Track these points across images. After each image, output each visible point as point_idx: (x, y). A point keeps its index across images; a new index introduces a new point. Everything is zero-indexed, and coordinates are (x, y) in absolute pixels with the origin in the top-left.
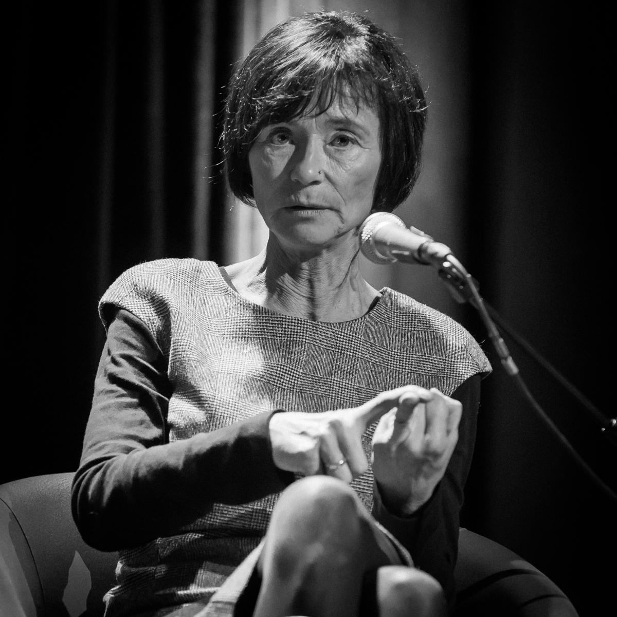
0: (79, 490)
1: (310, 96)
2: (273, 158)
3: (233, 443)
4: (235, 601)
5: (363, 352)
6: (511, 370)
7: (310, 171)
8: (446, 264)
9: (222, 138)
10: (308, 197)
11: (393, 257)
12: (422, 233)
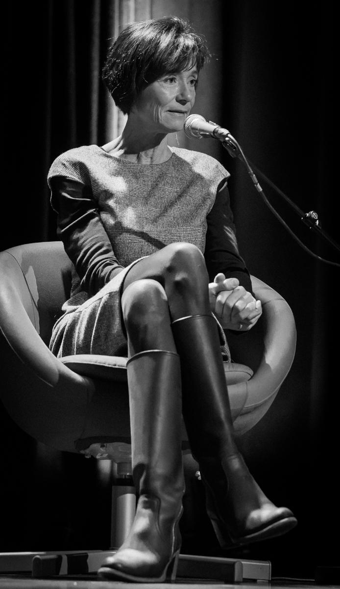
6: (259, 189)
8: (227, 139)
12: (215, 124)
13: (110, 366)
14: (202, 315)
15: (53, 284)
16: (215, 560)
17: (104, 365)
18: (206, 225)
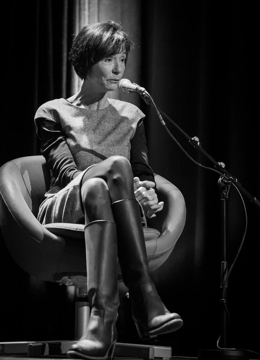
0: (61, 166)
8: (144, 93)
9: (219, 181)
11: (128, 92)
12: (137, 84)
17: (70, 229)
18: (130, 145)
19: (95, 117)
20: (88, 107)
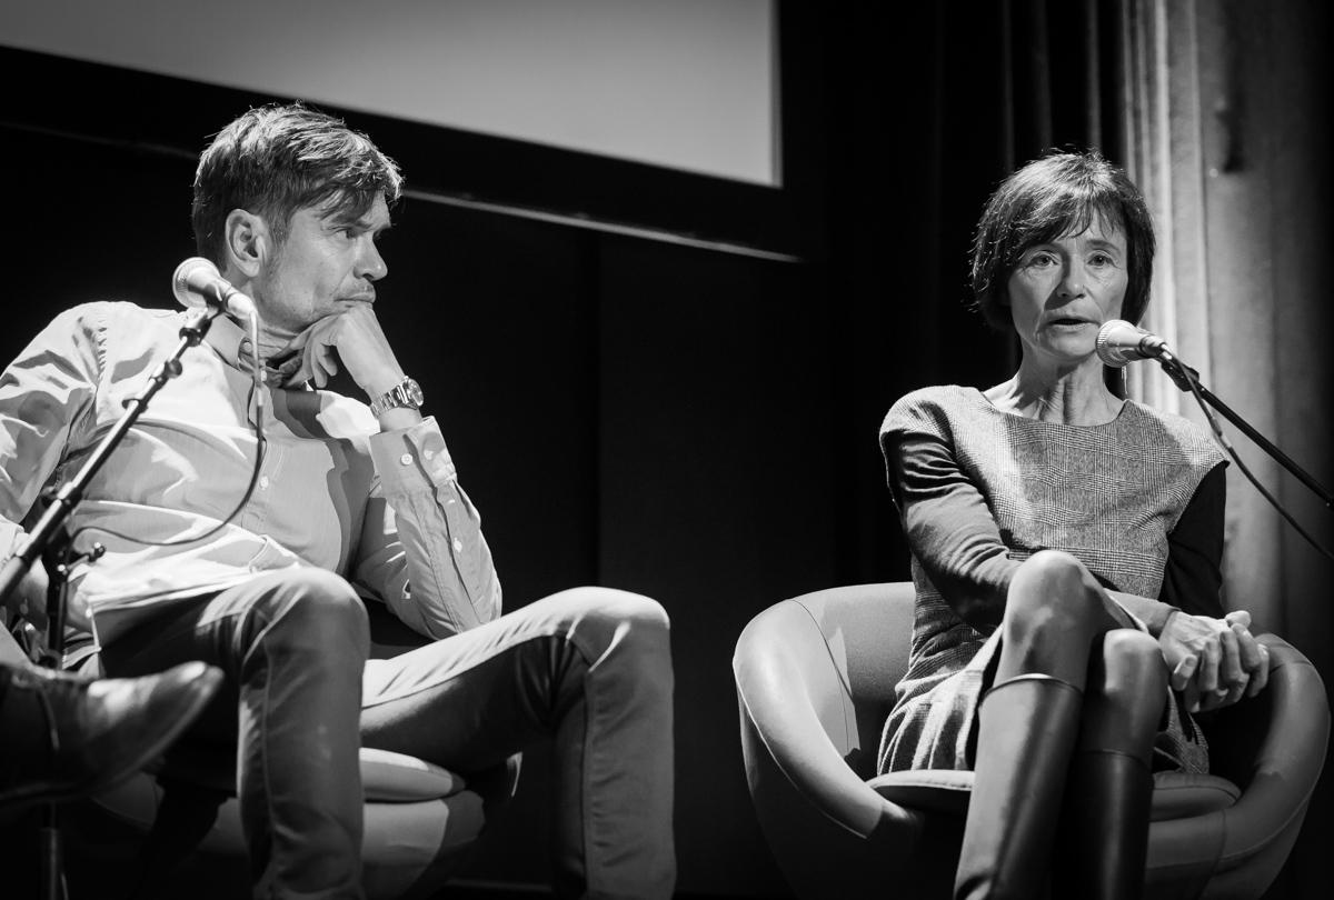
1: (1073, 215)
2: (1038, 278)
3: (112, 720)
4: (983, 669)
5: (1118, 451)
7: (1076, 286)
10: (1074, 310)
13: (955, 788)
14: (1129, 756)
15: (886, 658)
16: (1125, 145)
18: (1166, 549)
19: (1063, 448)
20: (262, 145)
